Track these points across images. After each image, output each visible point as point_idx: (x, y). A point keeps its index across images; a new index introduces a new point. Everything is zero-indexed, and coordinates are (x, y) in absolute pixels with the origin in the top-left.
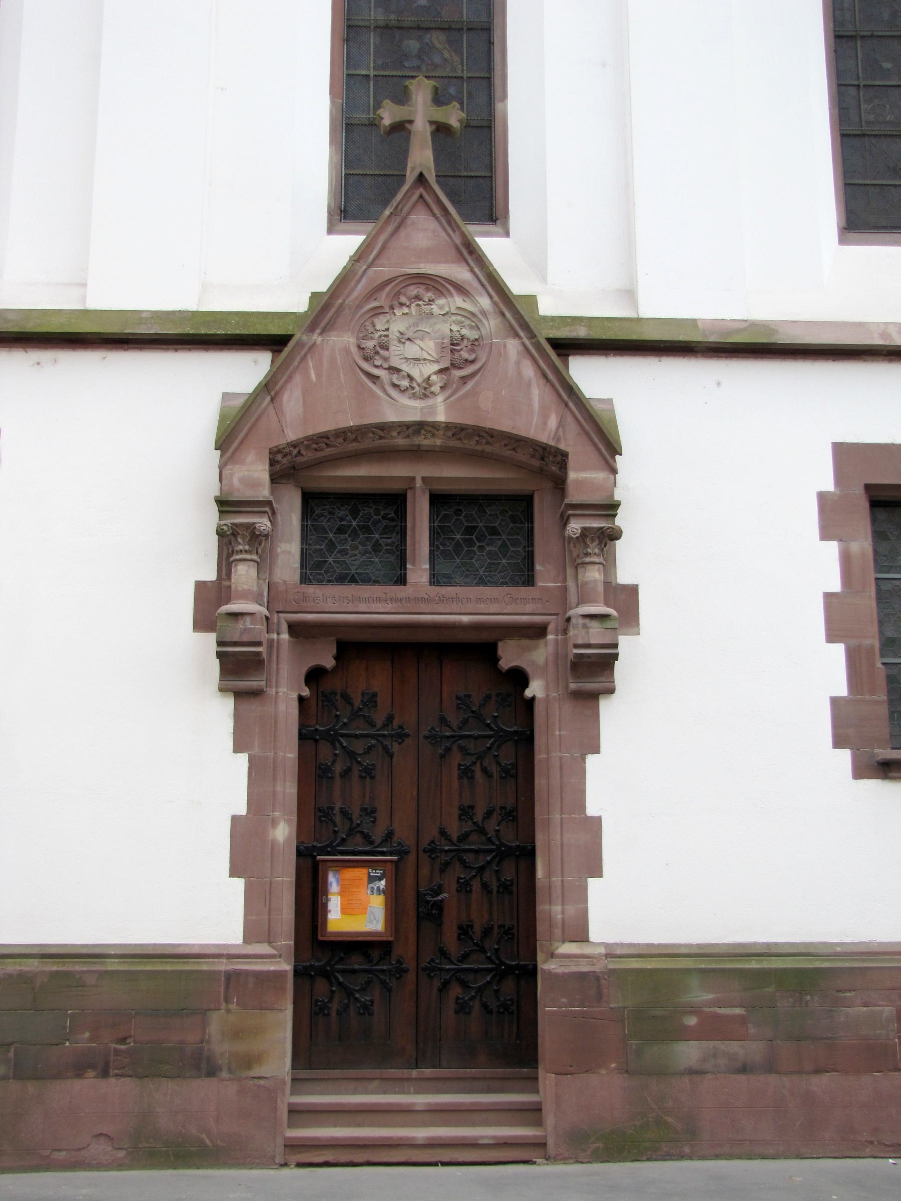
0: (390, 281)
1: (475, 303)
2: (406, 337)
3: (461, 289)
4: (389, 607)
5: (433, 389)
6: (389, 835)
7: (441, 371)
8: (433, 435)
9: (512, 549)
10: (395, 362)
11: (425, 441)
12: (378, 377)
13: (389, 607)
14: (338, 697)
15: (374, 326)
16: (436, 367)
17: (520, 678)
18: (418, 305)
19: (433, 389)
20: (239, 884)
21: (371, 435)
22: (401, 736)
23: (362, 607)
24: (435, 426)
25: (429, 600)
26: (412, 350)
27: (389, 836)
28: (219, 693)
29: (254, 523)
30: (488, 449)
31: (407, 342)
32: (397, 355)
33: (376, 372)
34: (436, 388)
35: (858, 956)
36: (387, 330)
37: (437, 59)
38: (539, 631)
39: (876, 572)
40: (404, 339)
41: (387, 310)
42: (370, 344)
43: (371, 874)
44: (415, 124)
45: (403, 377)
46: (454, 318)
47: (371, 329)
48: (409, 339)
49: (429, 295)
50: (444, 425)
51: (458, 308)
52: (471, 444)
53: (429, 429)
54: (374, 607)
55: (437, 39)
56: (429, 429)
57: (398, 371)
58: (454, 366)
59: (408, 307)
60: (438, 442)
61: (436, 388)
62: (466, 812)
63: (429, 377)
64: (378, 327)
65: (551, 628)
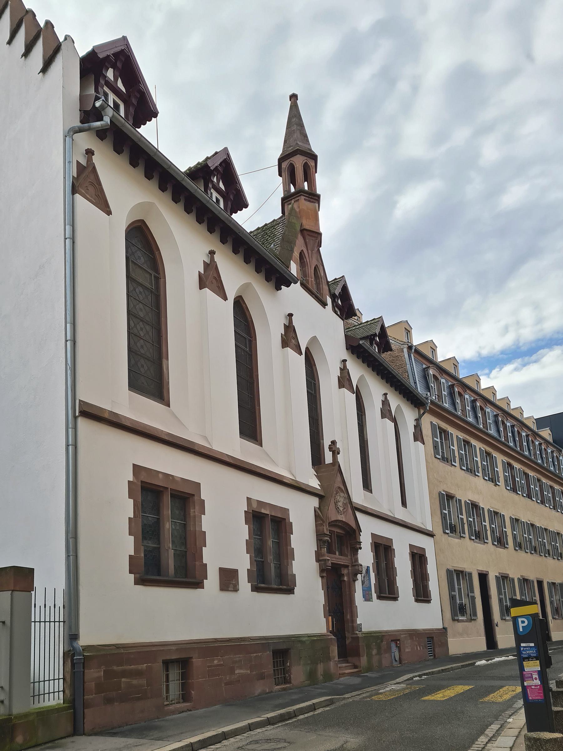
38: (347, 567)
57: (339, 508)
65: (350, 566)
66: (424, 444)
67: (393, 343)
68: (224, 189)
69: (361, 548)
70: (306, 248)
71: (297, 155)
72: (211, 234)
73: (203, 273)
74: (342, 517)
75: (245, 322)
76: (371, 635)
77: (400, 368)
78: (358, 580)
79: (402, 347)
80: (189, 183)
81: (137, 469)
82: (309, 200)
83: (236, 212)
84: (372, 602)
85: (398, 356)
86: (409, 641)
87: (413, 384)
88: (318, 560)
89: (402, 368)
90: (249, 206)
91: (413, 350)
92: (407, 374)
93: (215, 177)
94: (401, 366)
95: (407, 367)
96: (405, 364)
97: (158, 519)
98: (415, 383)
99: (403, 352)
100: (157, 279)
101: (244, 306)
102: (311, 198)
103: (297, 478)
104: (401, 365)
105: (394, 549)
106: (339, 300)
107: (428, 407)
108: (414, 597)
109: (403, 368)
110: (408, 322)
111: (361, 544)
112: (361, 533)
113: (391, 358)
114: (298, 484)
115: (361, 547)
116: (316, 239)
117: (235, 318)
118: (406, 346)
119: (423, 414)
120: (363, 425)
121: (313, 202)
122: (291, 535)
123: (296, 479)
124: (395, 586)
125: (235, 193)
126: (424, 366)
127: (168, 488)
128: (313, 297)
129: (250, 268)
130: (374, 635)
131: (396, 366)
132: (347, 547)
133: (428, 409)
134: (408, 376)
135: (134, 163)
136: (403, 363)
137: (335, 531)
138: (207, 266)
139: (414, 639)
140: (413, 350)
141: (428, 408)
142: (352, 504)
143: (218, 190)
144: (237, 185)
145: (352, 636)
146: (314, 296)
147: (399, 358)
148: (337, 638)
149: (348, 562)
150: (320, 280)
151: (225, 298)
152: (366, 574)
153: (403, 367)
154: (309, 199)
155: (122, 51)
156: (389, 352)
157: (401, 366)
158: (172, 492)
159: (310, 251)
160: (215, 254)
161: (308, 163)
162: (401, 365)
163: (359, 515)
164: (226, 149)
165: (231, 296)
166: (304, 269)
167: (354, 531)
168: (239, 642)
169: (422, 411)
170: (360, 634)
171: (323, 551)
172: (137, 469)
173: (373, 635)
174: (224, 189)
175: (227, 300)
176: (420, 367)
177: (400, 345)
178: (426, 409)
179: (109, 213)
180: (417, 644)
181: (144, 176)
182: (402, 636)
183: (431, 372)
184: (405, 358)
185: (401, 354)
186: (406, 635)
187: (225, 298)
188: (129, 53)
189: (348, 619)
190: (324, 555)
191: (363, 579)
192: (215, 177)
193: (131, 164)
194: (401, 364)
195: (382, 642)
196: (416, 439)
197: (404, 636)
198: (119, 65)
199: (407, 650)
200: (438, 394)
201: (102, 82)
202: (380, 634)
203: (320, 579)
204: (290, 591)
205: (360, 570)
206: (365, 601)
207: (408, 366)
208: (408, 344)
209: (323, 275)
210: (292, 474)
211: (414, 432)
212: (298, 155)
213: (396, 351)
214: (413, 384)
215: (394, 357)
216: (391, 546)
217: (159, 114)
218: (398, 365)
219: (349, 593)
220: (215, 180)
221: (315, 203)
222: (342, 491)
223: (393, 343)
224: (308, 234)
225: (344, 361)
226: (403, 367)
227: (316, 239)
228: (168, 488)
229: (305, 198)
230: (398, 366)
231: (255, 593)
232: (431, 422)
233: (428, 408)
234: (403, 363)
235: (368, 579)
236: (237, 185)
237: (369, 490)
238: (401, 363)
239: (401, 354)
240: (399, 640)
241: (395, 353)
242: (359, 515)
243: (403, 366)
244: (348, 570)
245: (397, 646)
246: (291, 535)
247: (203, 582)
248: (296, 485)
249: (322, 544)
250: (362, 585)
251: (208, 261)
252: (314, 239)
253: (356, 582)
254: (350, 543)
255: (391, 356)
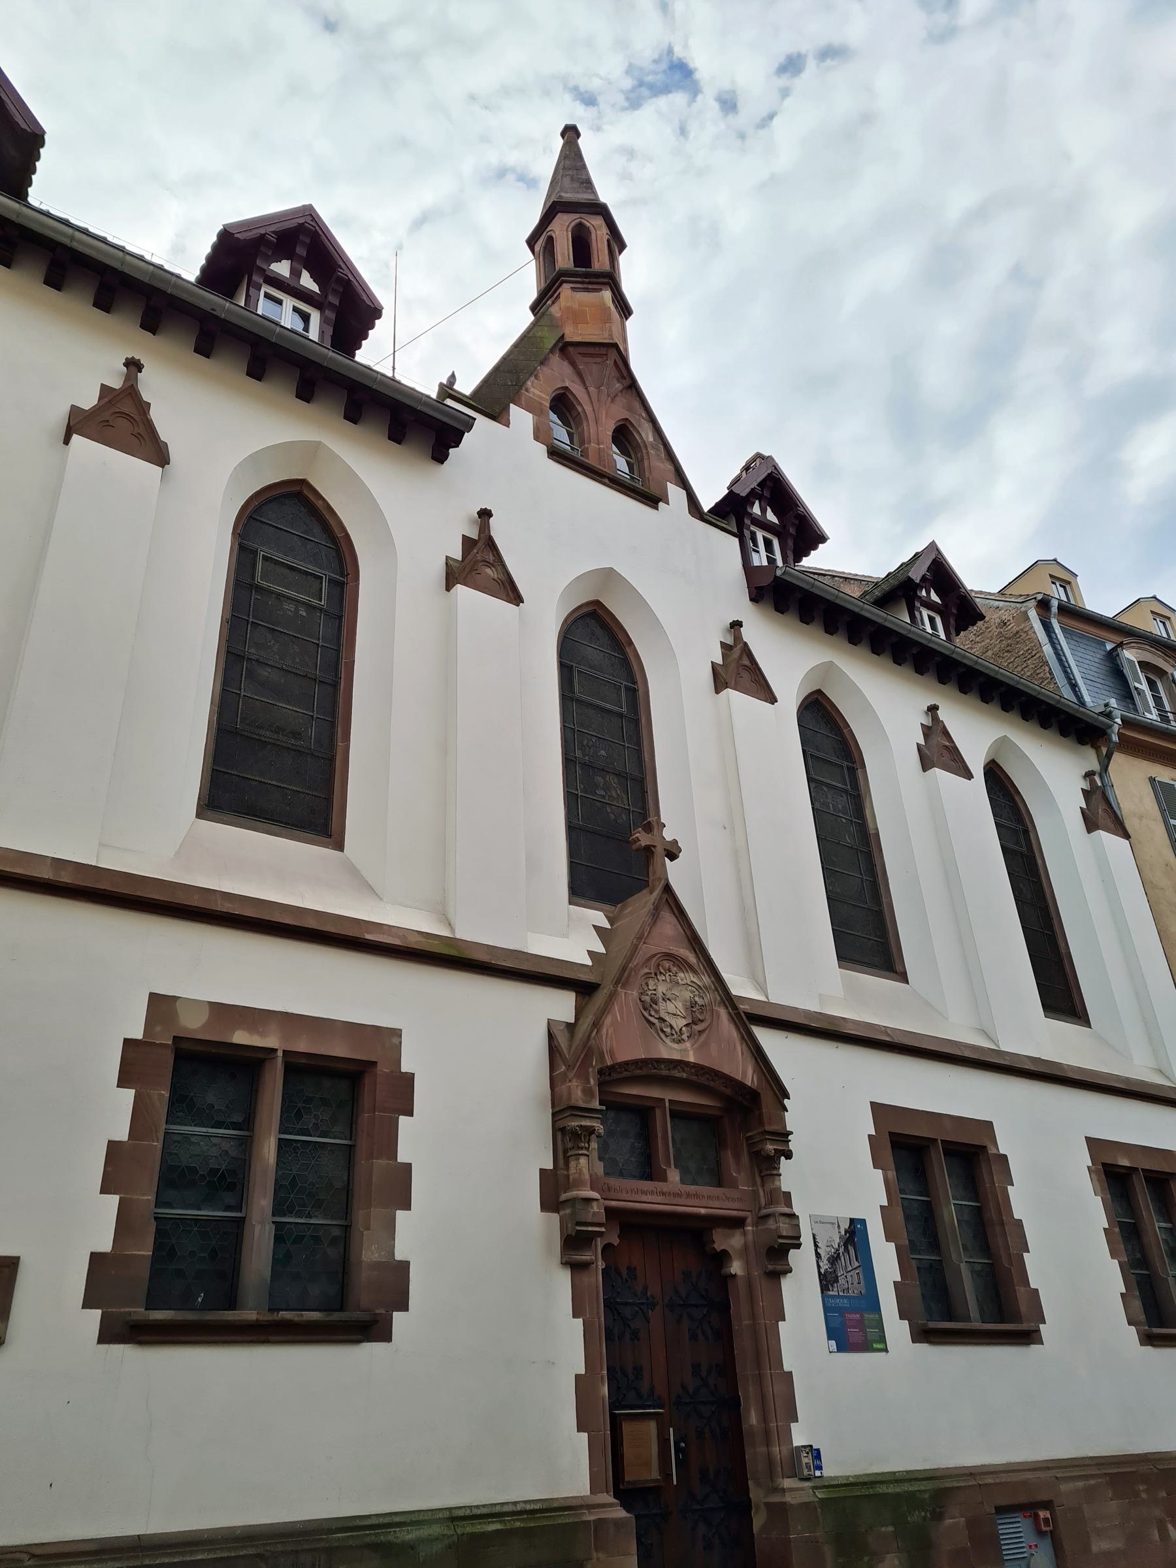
0: (654, 956)
1: (701, 979)
2: (667, 997)
3: (692, 969)
4: (659, 1199)
5: (683, 1037)
6: (652, 1389)
7: (686, 1025)
8: (684, 1071)
9: (184, 1105)
10: (663, 1015)
11: (676, 1073)
12: (654, 1024)
13: (659, 1199)
14: (613, 1269)
15: (648, 986)
16: (685, 1022)
17: (723, 1257)
18: (670, 975)
19: (683, 1037)
20: (584, 1436)
21: (651, 1066)
22: (653, 1306)
23: (644, 1198)
24: (687, 1064)
25: (679, 1195)
26: (671, 1007)
27: (652, 1389)
28: (561, 1265)
29: (594, 1126)
30: (712, 1084)
31: (668, 1001)
32: (665, 1008)
33: (652, 1019)
34: (685, 1037)
35: (245, 1547)
36: (655, 990)
37: (614, 794)
38: (737, 1223)
39: (280, 1132)
40: (666, 999)
41: (653, 976)
42: (647, 999)
43: (877, 1316)
44: (657, 848)
45: (667, 1026)
46: (690, 988)
47: (646, 988)
48: (668, 999)
49: (675, 969)
50: (692, 1064)
51: (692, 981)
52: (703, 1080)
53: (683, 1066)
54: (649, 1198)
55: (613, 780)
56: (683, 1066)
57: (664, 1021)
58: (694, 1023)
59: (664, 975)
60: (685, 1075)
61: (685, 1037)
62: (696, 1368)
63: (681, 1028)
64: (650, 988)
65: (749, 1220)
66: (1127, 836)
67: (1000, 606)
68: (939, 602)
69: (789, 1155)
70: (580, 383)
71: (557, 214)
72: (154, 335)
73: (924, 744)
74: (686, 1050)
75: (618, 653)
76: (871, 1491)
77: (1029, 659)
78: (791, 1272)
79: (1023, 609)
80: (212, 300)
81: (878, 1109)
82: (585, 288)
83: (807, 554)
84: (884, 1354)
85: (1017, 632)
86: (1113, 1506)
87: (1067, 693)
88: (550, 1202)
89: (1033, 656)
90: (384, 311)
91: (1054, 609)
92: (1047, 669)
93: (924, 590)
94: (1029, 654)
95: (1043, 652)
96: (1038, 644)
97: (928, 1204)
98: (1074, 686)
99: (1028, 619)
100: (852, 771)
101: (319, 504)
102: (589, 283)
103: (457, 932)
104: (1029, 652)
105: (1005, 1156)
106: (932, 591)
107: (1113, 735)
108: (1133, 1328)
109: (1035, 657)
110: (1058, 560)
111: (790, 1137)
112: (786, 1101)
113: (1004, 642)
114: (888, 1035)
115: (791, 1151)
116: (605, 358)
117: (801, 728)
118: (1033, 603)
119: (1109, 756)
120: (859, 796)
121: (595, 290)
122: (1009, 1187)
123: (999, 1048)
124: (1021, 1290)
125: (797, 522)
126: (1109, 646)
127: (937, 1140)
128: (604, 484)
129: (930, 680)
130: (890, 1491)
131: (1019, 657)
132: (737, 1157)
133: (1114, 739)
134: (1051, 673)
135: (256, 371)
136: (1032, 645)
137: (663, 1100)
138: (927, 731)
139: (1144, 1496)
140: (1054, 609)
141: (1115, 738)
142: (735, 1007)
143: (930, 605)
144: (798, 508)
145: (767, 1500)
146: (607, 481)
147: (1021, 636)
148: (636, 1517)
149: (736, 1205)
150: (644, 451)
151: (968, 775)
152: (842, 1250)
153: (1035, 655)
154: (585, 286)
155: (770, 475)
156: (980, 623)
157: (1029, 654)
158: (673, 1108)
159: (591, 389)
160: (141, 372)
161: (586, 223)
162: (1029, 652)
163: (767, 1038)
164: (933, 546)
165: (790, 693)
166: (580, 430)
167: (753, 1096)
168: (178, 1553)
169: (1104, 750)
170: (802, 1489)
171: (572, 1171)
172: (878, 1109)
173: (882, 1489)
174: (939, 602)
175: (777, 702)
176: (1100, 652)
177: (1018, 605)
178: (1110, 740)
179: (515, 597)
180: (1157, 1512)
181: (870, 652)
182: (1064, 1487)
183: (1130, 655)
184: (1034, 632)
185: (1023, 625)
186: (1092, 1482)
187: (968, 775)
188: (317, 228)
189: (752, 1426)
190: (578, 1184)
191: (825, 1266)
192: (924, 590)
193: (895, 662)
194: (1029, 649)
195: (938, 1516)
196: (1091, 825)
197: (1080, 1484)
198: (767, 493)
199: (1100, 1545)
200: (1173, 711)
201: (747, 521)
202: (923, 1486)
203: (564, 1279)
204: (1029, 1337)
205: (785, 1234)
206: (841, 1348)
207: (1047, 649)
208: (1035, 598)
209: (651, 439)
210: (447, 919)
211: (1084, 806)
212: (559, 215)
213: (1012, 621)
214: (1067, 693)
215: (1010, 638)
216: (986, 1147)
217: (383, 311)
218: (1021, 653)
219: (751, 1322)
220: (924, 593)
221: (601, 290)
222: (683, 965)
223: (1000, 606)
224: (579, 354)
225: (736, 625)
226: (1035, 655)
227: (605, 358)
228: (937, 1140)
229: (572, 285)
230: (1022, 657)
231: (924, 1348)
232: (1152, 780)
233: (1115, 738)
234: (1032, 645)
235: (857, 1264)
236: (798, 508)
237: (896, 972)
238: (1028, 648)
239: (1023, 625)
240: (1047, 1505)
241: (1010, 627)
242: (769, 1040)
243: (1034, 653)
244: (745, 1234)
245: (1040, 1533)
246: (1009, 1187)
247: (1038, 1331)
248: (453, 952)
249: (570, 1145)
250: (824, 1288)
251: (729, 641)
252: (599, 360)
253: (787, 1285)
254: (748, 1139)
255: (1003, 638)
